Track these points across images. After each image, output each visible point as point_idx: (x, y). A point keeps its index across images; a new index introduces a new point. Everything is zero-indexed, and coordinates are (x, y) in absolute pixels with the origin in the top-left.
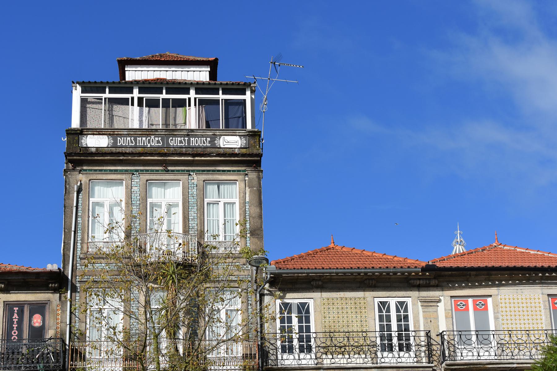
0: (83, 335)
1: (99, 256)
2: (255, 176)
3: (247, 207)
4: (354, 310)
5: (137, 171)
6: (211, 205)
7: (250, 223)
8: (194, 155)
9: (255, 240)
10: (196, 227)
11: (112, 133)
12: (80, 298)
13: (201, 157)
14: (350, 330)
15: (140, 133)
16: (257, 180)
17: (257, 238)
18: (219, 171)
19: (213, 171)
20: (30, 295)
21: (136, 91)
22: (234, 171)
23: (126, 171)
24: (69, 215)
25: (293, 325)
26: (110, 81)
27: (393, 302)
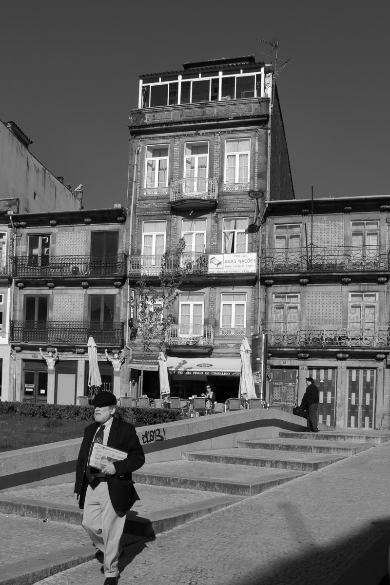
0: (139, 252)
1: (147, 198)
2: (263, 133)
3: (256, 157)
4: (333, 230)
5: (178, 136)
6: (243, 156)
7: (258, 168)
8: (195, 122)
9: (261, 181)
10: (218, 174)
11: (162, 110)
12: (138, 227)
13: (205, 122)
14: (330, 245)
15: (181, 108)
16: (265, 135)
17: (263, 179)
18: (237, 131)
19: (232, 131)
20: (106, 226)
21: (180, 77)
22: (247, 130)
23: (210, 133)
24: (124, 174)
25: (88, 345)
26: (161, 72)
27: (234, 304)
